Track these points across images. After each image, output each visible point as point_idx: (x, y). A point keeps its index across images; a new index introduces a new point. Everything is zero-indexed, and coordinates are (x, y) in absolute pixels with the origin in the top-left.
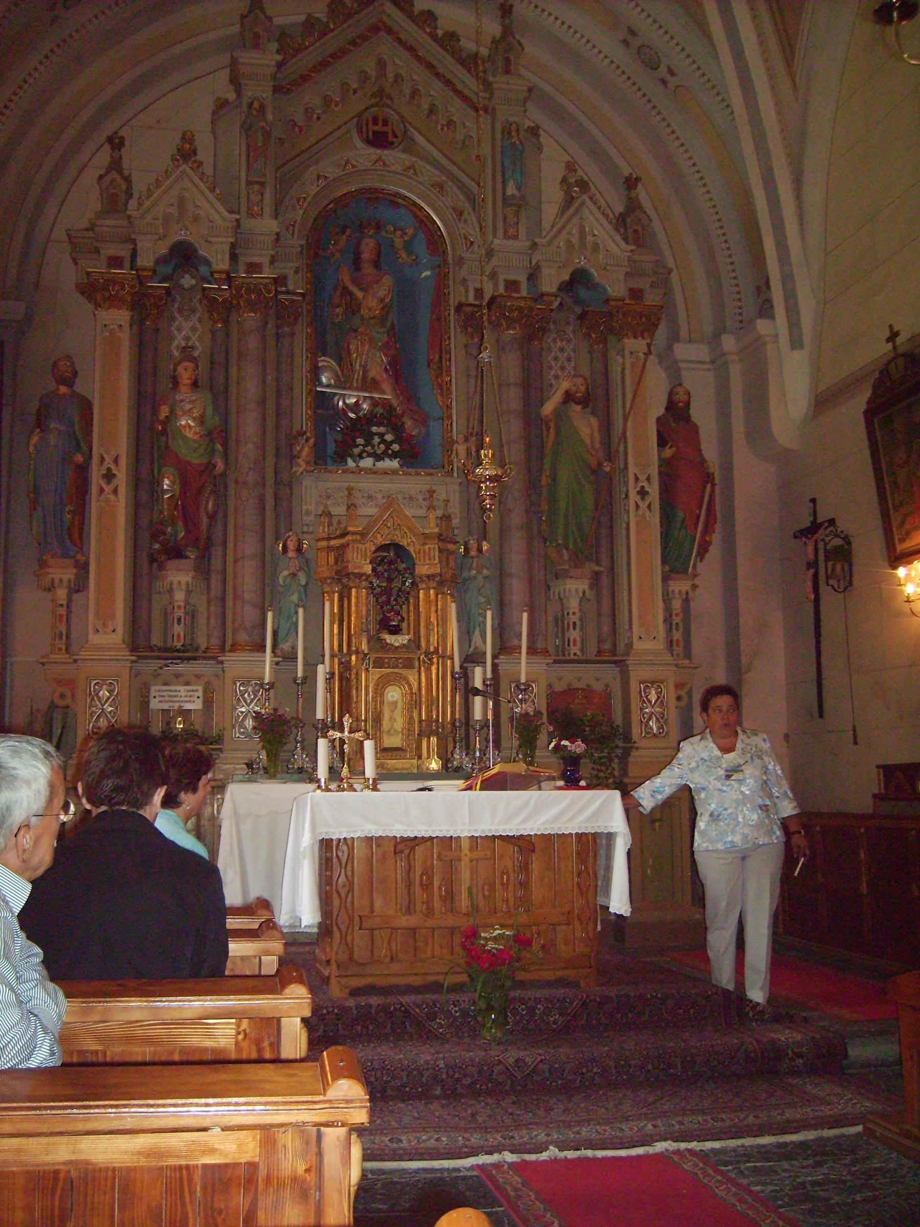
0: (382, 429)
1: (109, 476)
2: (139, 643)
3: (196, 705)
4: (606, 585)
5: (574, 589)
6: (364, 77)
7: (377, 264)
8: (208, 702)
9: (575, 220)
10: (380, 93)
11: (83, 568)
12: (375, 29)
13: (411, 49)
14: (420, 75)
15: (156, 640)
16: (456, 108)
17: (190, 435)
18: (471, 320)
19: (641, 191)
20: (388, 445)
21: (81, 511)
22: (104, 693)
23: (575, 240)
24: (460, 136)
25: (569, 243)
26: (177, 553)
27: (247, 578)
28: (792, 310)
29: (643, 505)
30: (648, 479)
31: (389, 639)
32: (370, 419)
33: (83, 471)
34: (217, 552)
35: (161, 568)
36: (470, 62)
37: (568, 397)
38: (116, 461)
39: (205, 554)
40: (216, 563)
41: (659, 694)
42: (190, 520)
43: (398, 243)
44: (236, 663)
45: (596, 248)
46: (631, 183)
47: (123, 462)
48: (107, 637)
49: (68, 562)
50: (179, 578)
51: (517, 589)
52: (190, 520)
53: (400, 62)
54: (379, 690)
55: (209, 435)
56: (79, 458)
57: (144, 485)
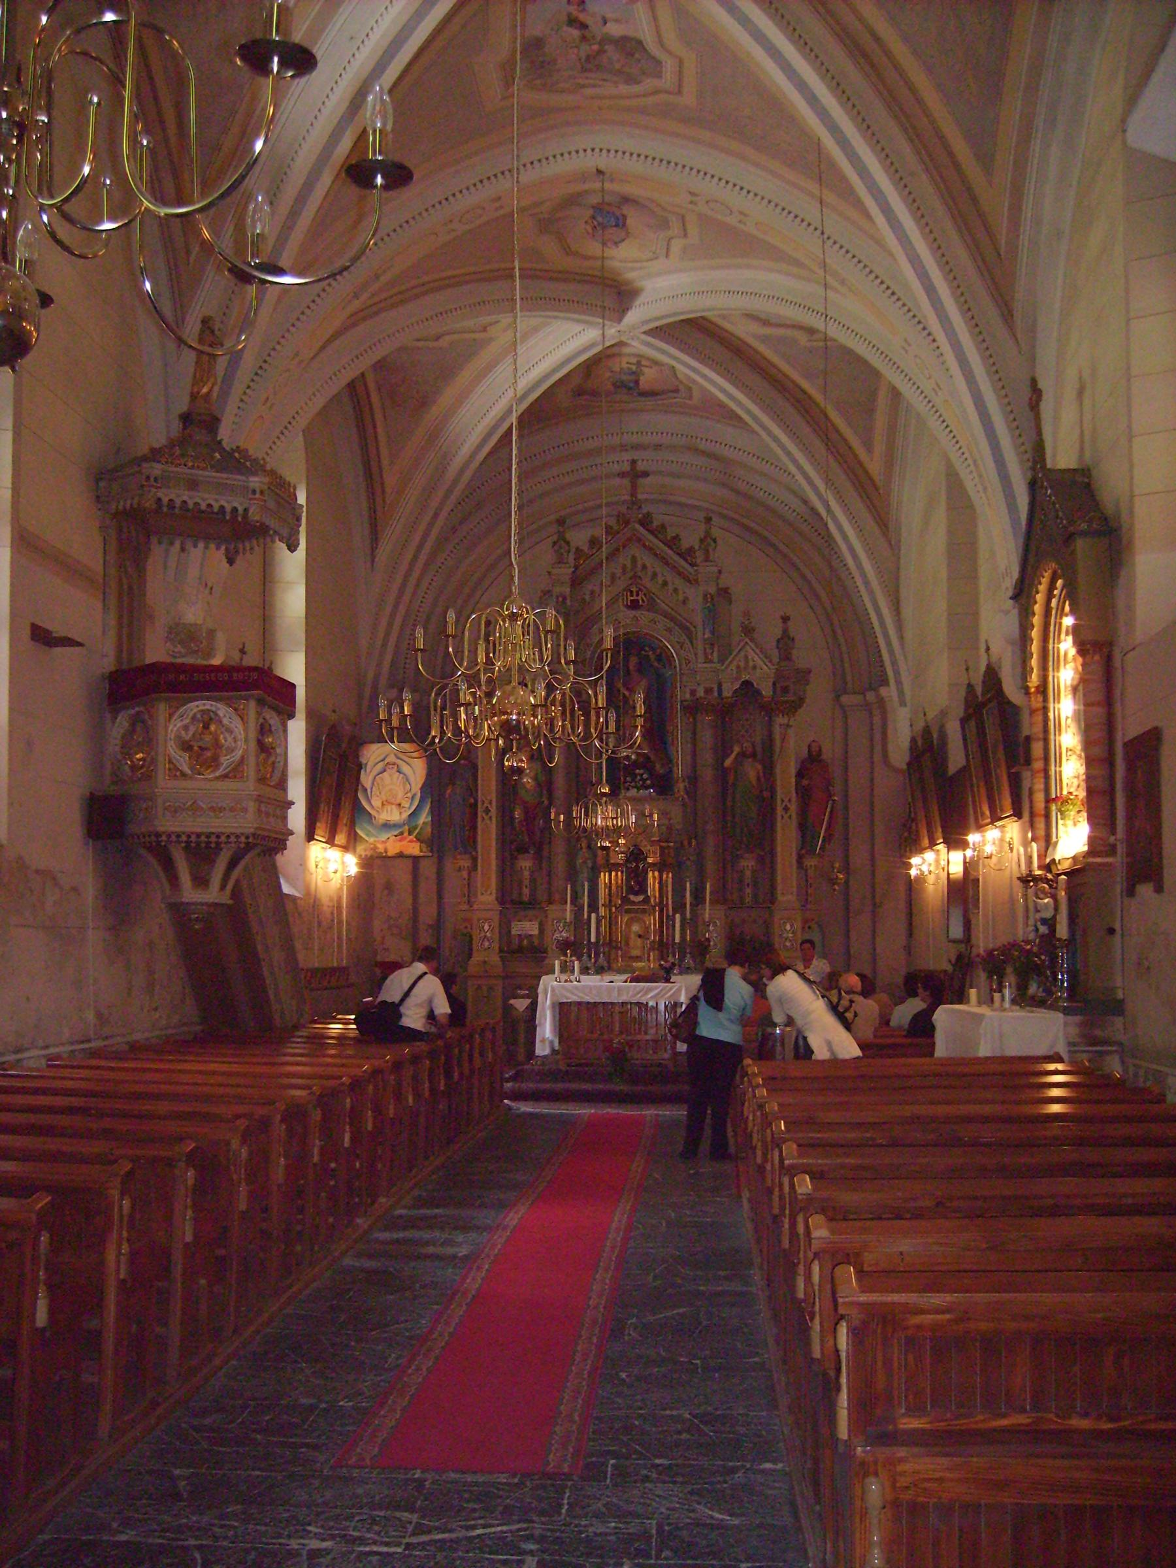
0: (642, 771)
1: (487, 811)
2: (502, 899)
3: (536, 932)
4: (767, 860)
5: (748, 863)
6: (624, 567)
7: (639, 670)
8: (542, 931)
9: (742, 654)
10: (635, 577)
11: (475, 860)
12: (629, 540)
13: (650, 549)
14: (659, 567)
15: (515, 896)
16: (679, 582)
17: (528, 786)
18: (693, 709)
19: (789, 623)
20: (644, 780)
21: (474, 827)
22: (486, 927)
23: (742, 664)
24: (681, 597)
25: (738, 667)
26: (523, 850)
27: (560, 865)
28: (899, 683)
29: (786, 816)
30: (790, 800)
31: (632, 897)
32: (635, 765)
33: (474, 806)
34: (546, 847)
35: (516, 858)
36: (687, 554)
37: (742, 755)
38: (490, 803)
39: (539, 848)
40: (545, 853)
41: (792, 926)
42: (531, 833)
43: (652, 657)
44: (553, 910)
45: (755, 667)
46: (785, 619)
47: (494, 804)
48: (487, 897)
49: (467, 856)
50: (525, 864)
51: (710, 866)
52: (531, 833)
53: (645, 558)
54: (629, 925)
55: (539, 785)
56: (472, 801)
57: (505, 813)
